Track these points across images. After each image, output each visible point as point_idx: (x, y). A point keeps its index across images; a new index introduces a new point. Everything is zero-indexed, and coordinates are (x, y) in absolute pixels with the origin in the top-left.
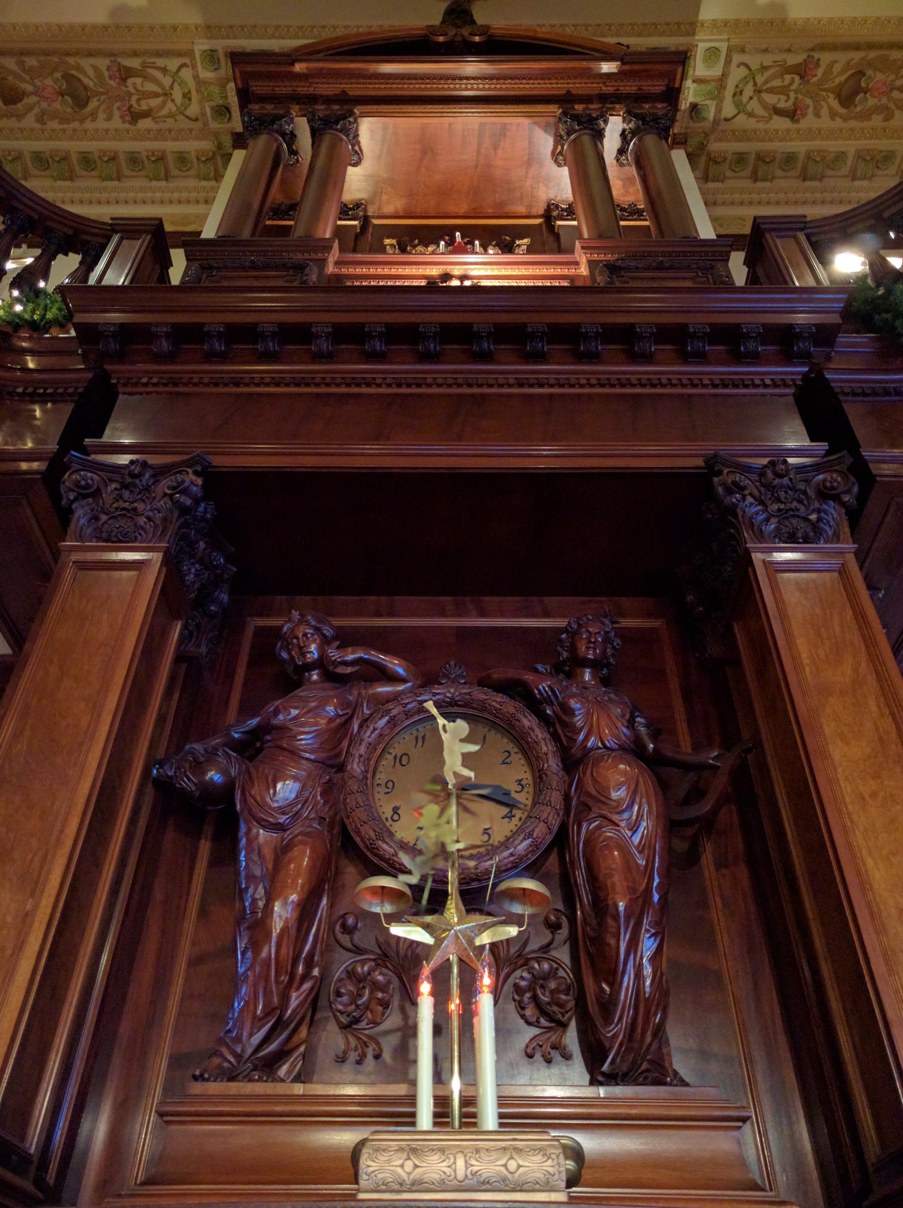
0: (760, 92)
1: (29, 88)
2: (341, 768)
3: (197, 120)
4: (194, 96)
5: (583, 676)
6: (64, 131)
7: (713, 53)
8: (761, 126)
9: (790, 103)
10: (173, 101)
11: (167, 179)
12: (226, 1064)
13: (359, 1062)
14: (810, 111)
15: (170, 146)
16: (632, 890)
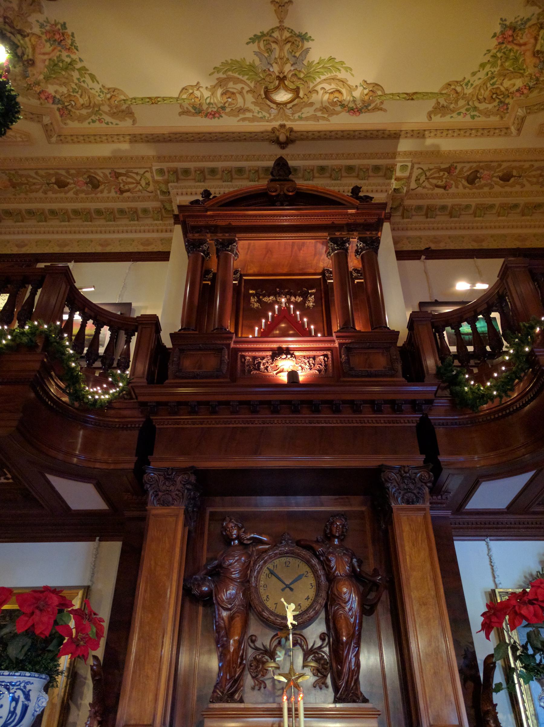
0: (428, 179)
1: (71, 181)
2: (248, 581)
3: (152, 192)
4: (151, 183)
5: (334, 541)
6: (87, 198)
7: (404, 167)
8: (430, 192)
9: (444, 182)
10: (141, 185)
11: (138, 220)
12: (219, 696)
13: (259, 690)
14: (453, 186)
15: (140, 205)
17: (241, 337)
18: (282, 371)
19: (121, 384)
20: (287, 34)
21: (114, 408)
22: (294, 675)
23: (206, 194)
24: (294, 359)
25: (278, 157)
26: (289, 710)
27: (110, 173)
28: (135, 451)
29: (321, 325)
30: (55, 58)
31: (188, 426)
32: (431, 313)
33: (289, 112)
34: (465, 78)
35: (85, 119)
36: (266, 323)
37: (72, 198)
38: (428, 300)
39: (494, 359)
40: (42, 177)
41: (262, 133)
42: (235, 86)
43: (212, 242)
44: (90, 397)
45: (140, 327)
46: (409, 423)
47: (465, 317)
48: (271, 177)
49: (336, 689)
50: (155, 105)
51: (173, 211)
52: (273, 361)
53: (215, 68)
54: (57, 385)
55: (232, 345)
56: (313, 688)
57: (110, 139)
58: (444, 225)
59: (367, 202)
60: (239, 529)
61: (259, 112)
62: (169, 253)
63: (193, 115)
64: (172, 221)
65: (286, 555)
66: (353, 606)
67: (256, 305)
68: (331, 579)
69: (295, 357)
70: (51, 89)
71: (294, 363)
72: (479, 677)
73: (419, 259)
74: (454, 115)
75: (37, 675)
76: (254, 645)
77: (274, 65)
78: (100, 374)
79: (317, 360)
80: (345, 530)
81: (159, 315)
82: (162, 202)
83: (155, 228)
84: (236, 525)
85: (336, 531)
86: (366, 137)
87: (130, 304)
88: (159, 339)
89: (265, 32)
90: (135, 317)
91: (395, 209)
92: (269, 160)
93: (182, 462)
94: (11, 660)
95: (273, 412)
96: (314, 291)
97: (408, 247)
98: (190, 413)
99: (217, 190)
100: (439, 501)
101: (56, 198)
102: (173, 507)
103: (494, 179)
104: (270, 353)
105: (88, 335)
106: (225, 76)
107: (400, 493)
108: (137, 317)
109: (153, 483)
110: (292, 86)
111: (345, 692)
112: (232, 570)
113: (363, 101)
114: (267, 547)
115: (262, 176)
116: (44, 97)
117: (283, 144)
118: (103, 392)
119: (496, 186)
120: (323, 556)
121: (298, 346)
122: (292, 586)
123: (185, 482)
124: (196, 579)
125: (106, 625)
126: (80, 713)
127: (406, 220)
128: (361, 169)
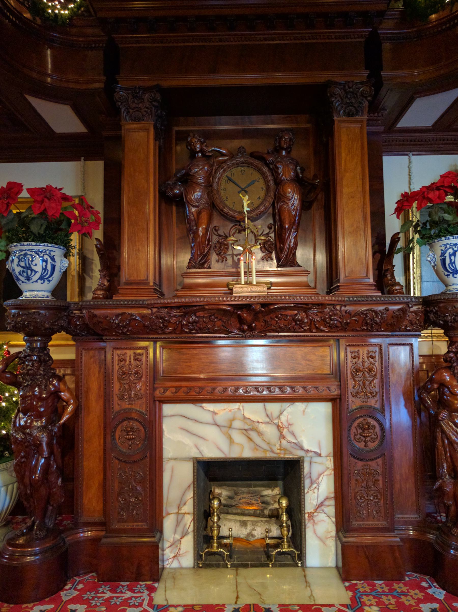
2: (211, 186)
5: (282, 153)
16: (290, 222)
22: (249, 245)
26: (245, 272)
44: (50, 11)
49: (278, 260)
56: (262, 261)
60: (202, 143)
65: (241, 165)
66: (295, 202)
68: (278, 183)
72: (386, 250)
75: (56, 246)
76: (218, 233)
80: (291, 143)
85: (284, 144)
94: (35, 235)
102: (143, 122)
109: (124, 101)
111: (285, 260)
112: (198, 176)
114: (226, 158)
120: (272, 165)
123: (151, 99)
124: (169, 184)
125: (101, 215)
126: (93, 281)
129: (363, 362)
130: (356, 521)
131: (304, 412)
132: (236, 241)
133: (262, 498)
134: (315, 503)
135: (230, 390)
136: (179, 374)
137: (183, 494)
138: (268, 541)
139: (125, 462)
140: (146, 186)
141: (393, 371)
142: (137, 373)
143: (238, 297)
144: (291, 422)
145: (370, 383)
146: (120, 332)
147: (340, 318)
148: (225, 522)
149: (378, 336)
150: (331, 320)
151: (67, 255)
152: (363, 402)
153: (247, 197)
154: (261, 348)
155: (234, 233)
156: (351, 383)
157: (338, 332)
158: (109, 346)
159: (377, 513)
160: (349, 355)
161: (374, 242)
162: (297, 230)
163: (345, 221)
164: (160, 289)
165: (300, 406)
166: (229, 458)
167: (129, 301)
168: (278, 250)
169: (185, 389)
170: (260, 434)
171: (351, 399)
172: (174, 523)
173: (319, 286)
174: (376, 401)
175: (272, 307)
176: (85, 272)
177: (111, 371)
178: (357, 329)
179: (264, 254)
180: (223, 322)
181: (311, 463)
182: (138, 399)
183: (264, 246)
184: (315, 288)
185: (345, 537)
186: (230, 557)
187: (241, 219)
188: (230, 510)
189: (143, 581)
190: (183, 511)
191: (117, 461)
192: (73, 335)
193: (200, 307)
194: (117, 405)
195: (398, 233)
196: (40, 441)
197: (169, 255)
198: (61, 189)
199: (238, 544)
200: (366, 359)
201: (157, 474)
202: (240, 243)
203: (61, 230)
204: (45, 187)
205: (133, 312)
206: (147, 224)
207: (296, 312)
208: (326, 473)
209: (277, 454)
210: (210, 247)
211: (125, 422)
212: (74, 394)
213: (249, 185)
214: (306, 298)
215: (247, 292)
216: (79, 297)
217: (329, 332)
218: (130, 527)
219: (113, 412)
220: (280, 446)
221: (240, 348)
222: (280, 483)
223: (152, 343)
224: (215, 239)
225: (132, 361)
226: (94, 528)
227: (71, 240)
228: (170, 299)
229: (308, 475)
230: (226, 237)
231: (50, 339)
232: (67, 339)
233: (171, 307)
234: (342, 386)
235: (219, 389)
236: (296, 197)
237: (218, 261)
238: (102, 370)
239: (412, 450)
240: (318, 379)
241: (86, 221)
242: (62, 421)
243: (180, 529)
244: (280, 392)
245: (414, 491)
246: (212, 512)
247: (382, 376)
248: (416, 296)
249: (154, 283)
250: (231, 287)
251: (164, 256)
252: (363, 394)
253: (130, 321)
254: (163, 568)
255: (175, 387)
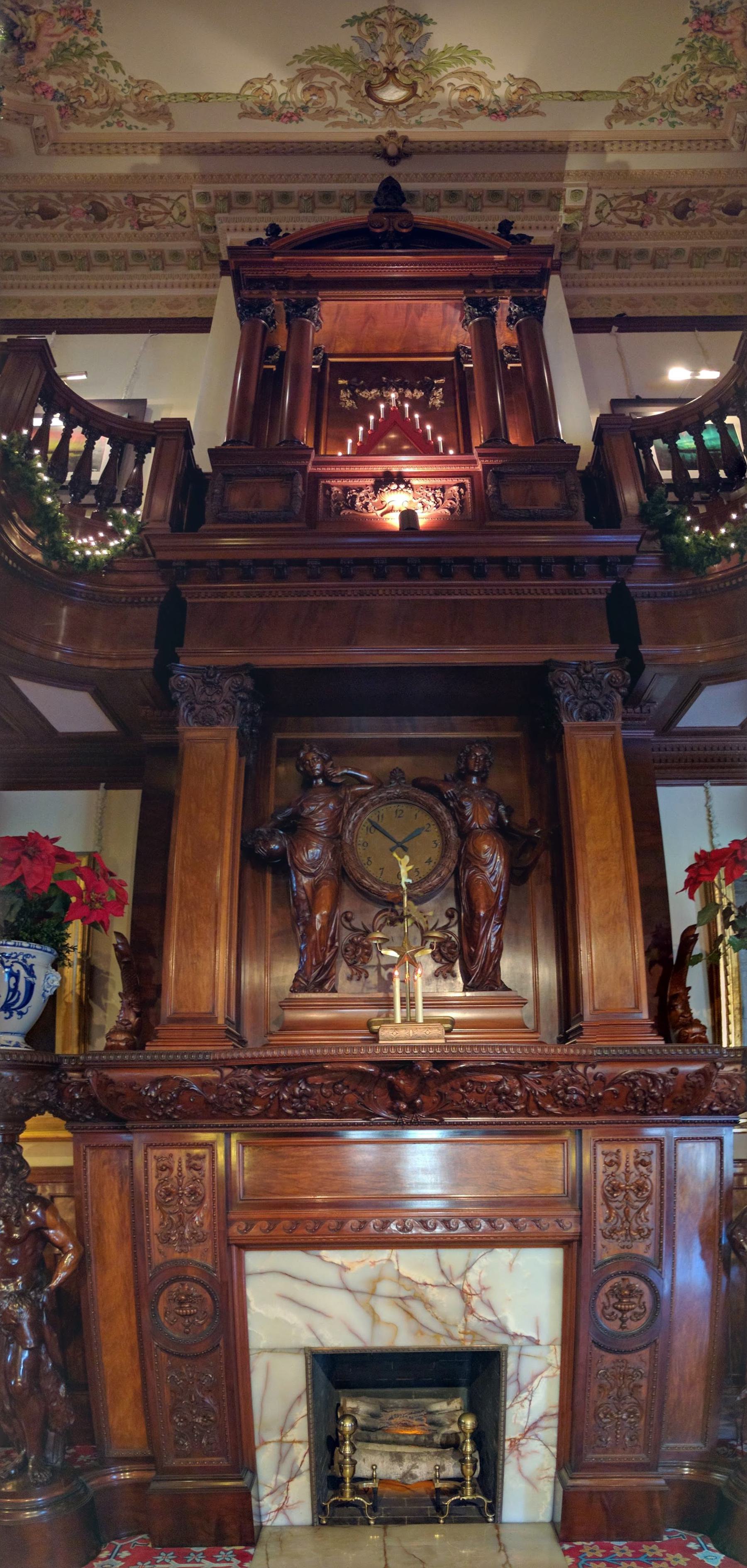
1: (64, 210)
2: (340, 837)
4: (188, 213)
6: (86, 235)
7: (576, 194)
8: (619, 229)
9: (639, 216)
11: (163, 269)
15: (168, 246)
16: (487, 906)
17: (325, 455)
18: (391, 510)
19: (127, 532)
20: (398, 16)
21: (117, 571)
22: (410, 948)
23: (273, 230)
24: (410, 491)
25: (385, 177)
26: (403, 1000)
27: (126, 199)
28: (153, 640)
29: (454, 435)
30: (67, 41)
31: (238, 600)
32: (630, 417)
33: (401, 115)
34: (653, 74)
35: (97, 121)
36: (364, 432)
37: (61, 235)
38: (625, 396)
39: (731, 490)
40: (18, 202)
41: (362, 143)
42: (323, 80)
43: (281, 303)
44: (77, 553)
45: (159, 439)
46: (595, 593)
47: (684, 423)
48: (374, 206)
49: (466, 977)
50: (204, 104)
51: (220, 255)
52: (376, 494)
53: (295, 56)
54: (22, 533)
55: (310, 468)
57: (131, 150)
58: (644, 279)
59: (524, 243)
60: (324, 762)
61: (357, 115)
62: (210, 320)
63: (260, 117)
64: (218, 270)
67: (349, 404)
68: (465, 833)
69: (412, 488)
70: (53, 81)
71: (410, 498)
73: (608, 331)
74: (645, 121)
75: (38, 946)
77: (381, 53)
78: (93, 515)
79: (448, 492)
80: (488, 764)
81: (191, 419)
82: (204, 241)
83: (191, 280)
84: (320, 756)
86: (516, 151)
87: (144, 401)
88: (190, 458)
89: (368, 13)
90: (152, 421)
91: (567, 254)
92: (372, 182)
93: (230, 657)
95: (376, 577)
96: (442, 381)
97: (589, 312)
98: (240, 579)
99: (291, 225)
100: (637, 716)
101: (37, 235)
102: (218, 727)
103: (715, 211)
104: (371, 481)
105: (74, 452)
106: (309, 67)
107: (576, 704)
108: (156, 423)
110: (406, 81)
113: (511, 102)
115: (361, 204)
116: (40, 91)
117: (393, 158)
118: (98, 544)
119: (718, 222)
121: (416, 470)
122: (405, 844)
124: (260, 833)
125: (129, 889)
127: (584, 272)
128: (512, 196)
129: (627, 1173)
130: (594, 1453)
131: (511, 1265)
132: (385, 940)
133: (430, 1417)
134: (523, 1423)
135: (372, 1224)
136: (274, 1194)
137: (290, 1410)
138: (439, 1485)
139: (179, 1355)
140: (217, 837)
141: (682, 1191)
142: (193, 1192)
143: (390, 1047)
144: (484, 1284)
145: (638, 1212)
146: (160, 1113)
147: (584, 1088)
148: (364, 1456)
149: (657, 1122)
150: (567, 1092)
151: (57, 964)
152: (623, 1247)
153: (407, 858)
154: (432, 1147)
155: (382, 926)
156: (601, 1212)
157: (579, 1115)
158: (138, 1140)
159: (631, 1440)
160: (600, 1159)
161: (649, 943)
162: (501, 921)
163: (593, 902)
164: (238, 1030)
165: (504, 1255)
166: (371, 1349)
167: (177, 1053)
168: (466, 958)
169: (287, 1223)
170: (428, 1305)
171: (600, 1241)
172: (276, 1458)
173: (543, 1027)
174: (648, 1246)
175: (454, 1067)
176: (91, 997)
177: (143, 1189)
178: (617, 1109)
179: (439, 965)
180: (360, 1095)
181: (520, 1356)
182: (197, 1241)
183: (440, 951)
184: (536, 1031)
185: (571, 1478)
186: (374, 1509)
187: (395, 899)
188: (373, 1436)
189: (228, 1546)
190: (289, 1438)
191: (164, 1355)
192: (68, 1120)
193: (315, 1067)
194: (157, 1253)
195: (693, 927)
196: (16, 1320)
197: (256, 966)
198: (56, 840)
199: (388, 1489)
200: (632, 1168)
201: (240, 1376)
202: (392, 945)
203: (50, 916)
204: (26, 835)
205: (184, 1074)
206: (217, 906)
207: (501, 1077)
208: (545, 1374)
209: (459, 1340)
210: (336, 952)
211: (174, 1285)
212: (75, 1232)
213: (411, 837)
214: (519, 1050)
215: (405, 1039)
216: (79, 1045)
217: (563, 1115)
218: (198, 1464)
219: (150, 1267)
220: (466, 1326)
221: (393, 1146)
222: (463, 1390)
223: (222, 1136)
224: (345, 935)
225: (184, 1170)
226: (135, 1467)
227: (68, 935)
228: (257, 1050)
229: (514, 1378)
230: (367, 932)
231: (23, 1128)
232: (56, 1128)
233: (259, 1067)
234: (584, 1216)
235: (352, 1223)
236: (498, 859)
237: (350, 978)
238: (127, 1187)
239: (707, 1333)
240: (539, 1205)
241: (98, 900)
242: (54, 1284)
243: (286, 1467)
244: (467, 1230)
245: (702, 1408)
246: (341, 1439)
247: (662, 1199)
248: (732, 1045)
249: (227, 1020)
250: (375, 1028)
251: (248, 967)
252: (624, 1232)
253: (178, 1092)
254: (261, 1527)
255: (268, 1220)
